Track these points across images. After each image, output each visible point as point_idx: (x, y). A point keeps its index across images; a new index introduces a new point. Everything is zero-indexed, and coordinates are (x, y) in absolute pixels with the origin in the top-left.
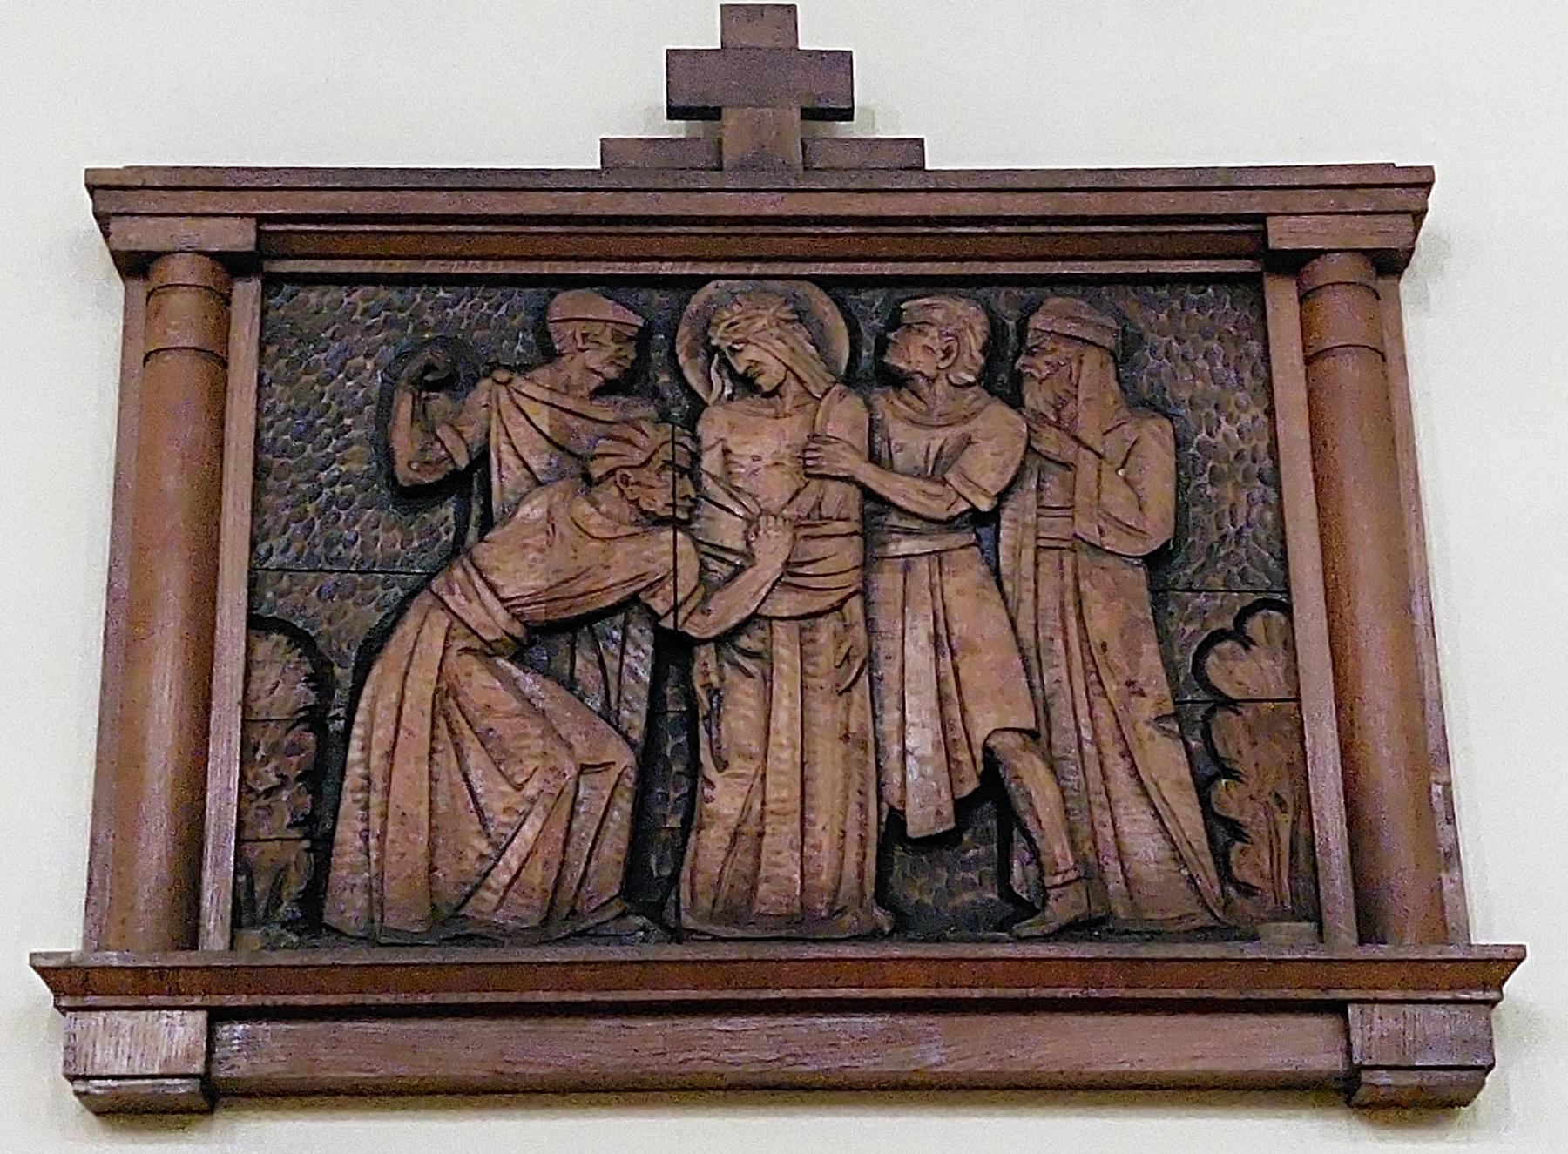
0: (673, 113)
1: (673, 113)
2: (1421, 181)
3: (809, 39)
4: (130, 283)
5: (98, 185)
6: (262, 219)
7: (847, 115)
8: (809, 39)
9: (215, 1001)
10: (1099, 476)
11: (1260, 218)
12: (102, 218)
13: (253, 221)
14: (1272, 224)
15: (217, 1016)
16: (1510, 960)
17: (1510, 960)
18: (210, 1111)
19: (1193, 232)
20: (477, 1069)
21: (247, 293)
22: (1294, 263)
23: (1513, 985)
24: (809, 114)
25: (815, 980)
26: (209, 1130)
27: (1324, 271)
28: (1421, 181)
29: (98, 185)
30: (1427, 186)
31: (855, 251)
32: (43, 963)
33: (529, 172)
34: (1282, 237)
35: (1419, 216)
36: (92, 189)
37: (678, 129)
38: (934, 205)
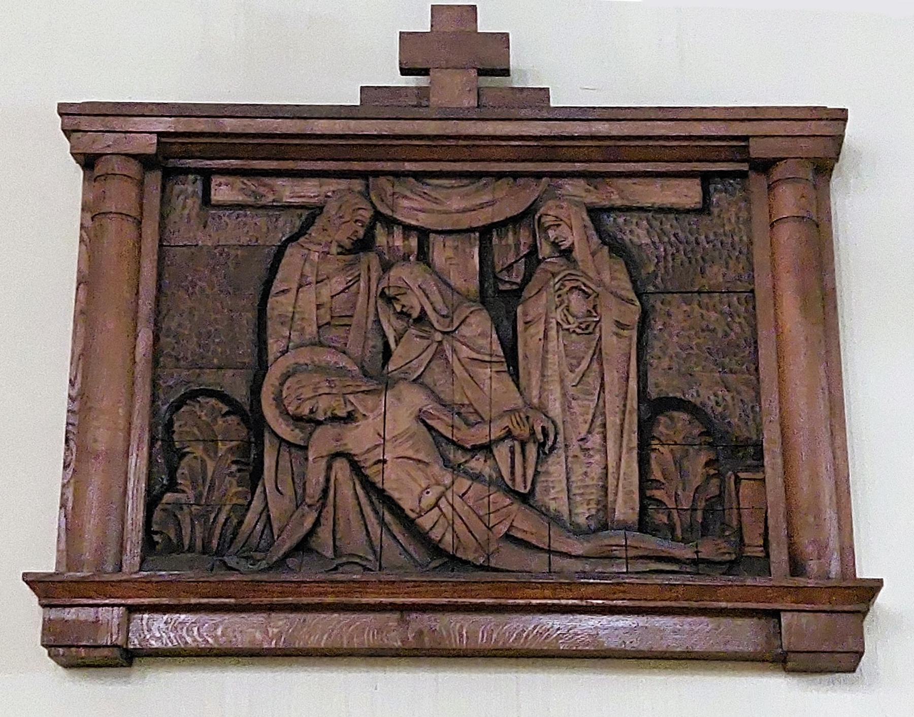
0: (404, 72)
1: (404, 72)
2: (841, 116)
3: (425, 26)
4: (87, 172)
5: (65, 111)
6: (160, 134)
7: (506, 72)
8: (425, 26)
9: (130, 601)
10: (335, 295)
11: (746, 138)
12: (68, 133)
13: (155, 137)
14: (752, 142)
15: (132, 609)
16: (873, 588)
17: (873, 588)
18: (130, 664)
19: (321, 145)
20: (369, 640)
21: (154, 179)
22: (765, 166)
23: (882, 598)
24: (482, 72)
25: (565, 595)
26: (128, 676)
27: (778, 172)
28: (841, 116)
29: (65, 111)
30: (845, 120)
31: (321, 155)
32: (29, 579)
33: (714, 108)
34: (758, 150)
35: (839, 139)
36: (61, 115)
37: (411, 81)
38: (557, 128)
